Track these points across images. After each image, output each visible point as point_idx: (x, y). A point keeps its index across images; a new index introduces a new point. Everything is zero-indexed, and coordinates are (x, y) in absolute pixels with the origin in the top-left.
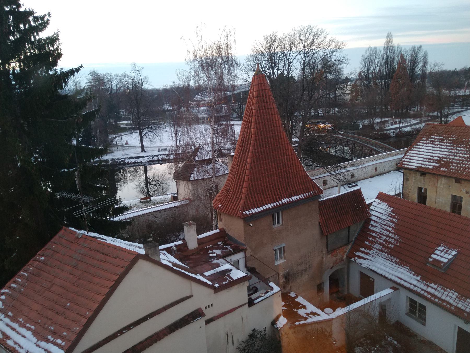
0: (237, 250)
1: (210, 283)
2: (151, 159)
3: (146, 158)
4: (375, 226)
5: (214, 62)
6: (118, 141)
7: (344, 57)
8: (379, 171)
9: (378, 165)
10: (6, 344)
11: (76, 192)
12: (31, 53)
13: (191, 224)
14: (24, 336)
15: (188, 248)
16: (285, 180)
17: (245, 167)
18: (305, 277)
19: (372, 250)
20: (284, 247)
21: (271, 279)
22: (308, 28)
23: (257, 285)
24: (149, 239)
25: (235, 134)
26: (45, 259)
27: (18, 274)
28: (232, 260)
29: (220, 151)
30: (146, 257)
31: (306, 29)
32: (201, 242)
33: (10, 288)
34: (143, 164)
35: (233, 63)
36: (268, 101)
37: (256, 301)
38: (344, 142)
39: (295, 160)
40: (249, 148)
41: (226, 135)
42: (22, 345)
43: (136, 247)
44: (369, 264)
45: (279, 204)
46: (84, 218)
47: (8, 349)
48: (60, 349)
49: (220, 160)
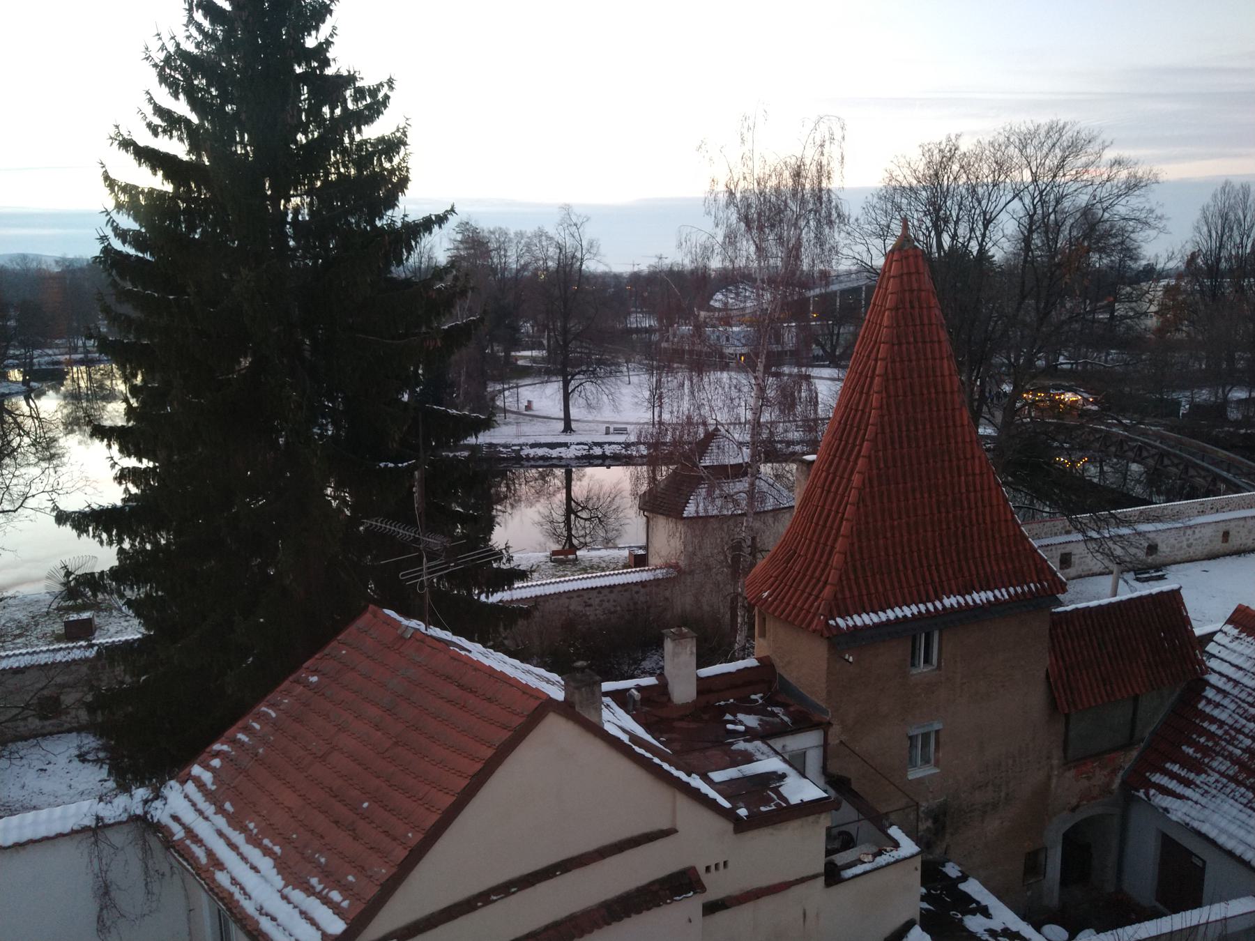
0: (802, 722)
1: (727, 804)
2: (585, 453)
3: (573, 447)
4: (1217, 705)
5: (780, 211)
6: (507, 399)
7: (1151, 211)
8: (1235, 542)
9: (1233, 524)
10: (214, 880)
11: (409, 522)
12: (339, 174)
13: (683, 636)
14: (255, 869)
15: (669, 699)
16: (957, 543)
17: (843, 496)
18: (993, 826)
19: (1206, 772)
20: (937, 732)
21: (893, 817)
22: (1051, 128)
23: (852, 829)
24: (579, 664)
25: (816, 403)
26: (317, 684)
27: (255, 710)
28: (788, 749)
29: (771, 441)
30: (566, 709)
31: (1043, 132)
32: (704, 686)
33: (233, 742)
34: (563, 463)
35: (830, 214)
36: (926, 321)
37: (848, 873)
38: (1131, 449)
39: (990, 489)
40: (861, 445)
41: (792, 406)
42: (248, 889)
43: (540, 677)
44: (1193, 813)
45: (935, 608)
46: (422, 587)
47: (217, 894)
48: (336, 917)
49: (766, 469)
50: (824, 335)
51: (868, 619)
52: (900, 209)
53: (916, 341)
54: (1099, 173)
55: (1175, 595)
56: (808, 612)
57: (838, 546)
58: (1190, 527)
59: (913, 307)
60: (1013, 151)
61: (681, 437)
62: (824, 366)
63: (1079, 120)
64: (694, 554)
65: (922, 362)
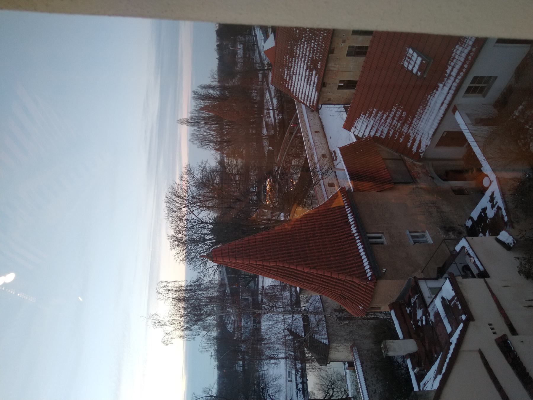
0: (417, 290)
1: (461, 326)
2: (301, 393)
4: (382, 132)
5: (195, 306)
7: (200, 166)
8: (319, 129)
9: (312, 130)
13: (385, 347)
15: (416, 352)
20: (410, 232)
22: (167, 202)
23: (460, 267)
25: (274, 285)
28: (429, 296)
29: (292, 305)
35: (196, 285)
41: (275, 296)
44: (426, 137)
45: (357, 236)
49: (303, 305)
50: (245, 281)
51: (366, 263)
52: (195, 256)
53: (249, 249)
54: (184, 184)
55: (341, 149)
56: (366, 289)
57: (335, 277)
58: (315, 145)
59: (235, 251)
60: (175, 215)
61: (292, 347)
62: (258, 280)
63: (165, 193)
64: (345, 339)
65: (257, 246)
